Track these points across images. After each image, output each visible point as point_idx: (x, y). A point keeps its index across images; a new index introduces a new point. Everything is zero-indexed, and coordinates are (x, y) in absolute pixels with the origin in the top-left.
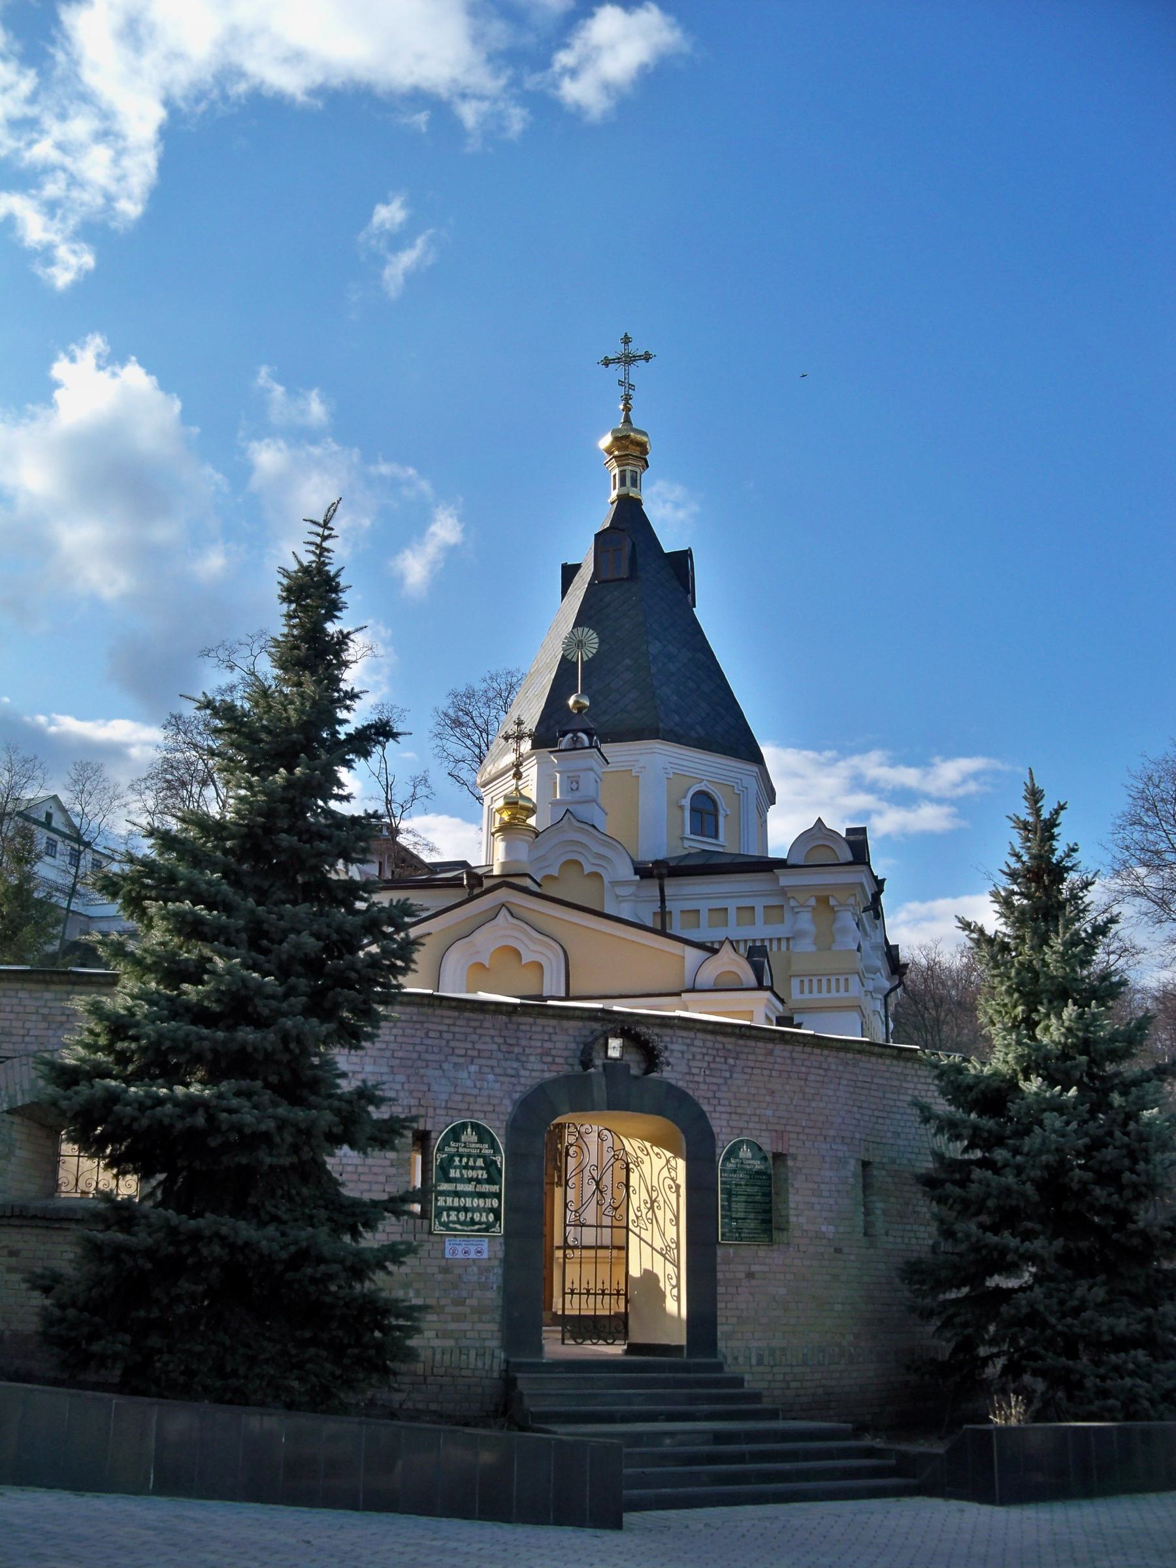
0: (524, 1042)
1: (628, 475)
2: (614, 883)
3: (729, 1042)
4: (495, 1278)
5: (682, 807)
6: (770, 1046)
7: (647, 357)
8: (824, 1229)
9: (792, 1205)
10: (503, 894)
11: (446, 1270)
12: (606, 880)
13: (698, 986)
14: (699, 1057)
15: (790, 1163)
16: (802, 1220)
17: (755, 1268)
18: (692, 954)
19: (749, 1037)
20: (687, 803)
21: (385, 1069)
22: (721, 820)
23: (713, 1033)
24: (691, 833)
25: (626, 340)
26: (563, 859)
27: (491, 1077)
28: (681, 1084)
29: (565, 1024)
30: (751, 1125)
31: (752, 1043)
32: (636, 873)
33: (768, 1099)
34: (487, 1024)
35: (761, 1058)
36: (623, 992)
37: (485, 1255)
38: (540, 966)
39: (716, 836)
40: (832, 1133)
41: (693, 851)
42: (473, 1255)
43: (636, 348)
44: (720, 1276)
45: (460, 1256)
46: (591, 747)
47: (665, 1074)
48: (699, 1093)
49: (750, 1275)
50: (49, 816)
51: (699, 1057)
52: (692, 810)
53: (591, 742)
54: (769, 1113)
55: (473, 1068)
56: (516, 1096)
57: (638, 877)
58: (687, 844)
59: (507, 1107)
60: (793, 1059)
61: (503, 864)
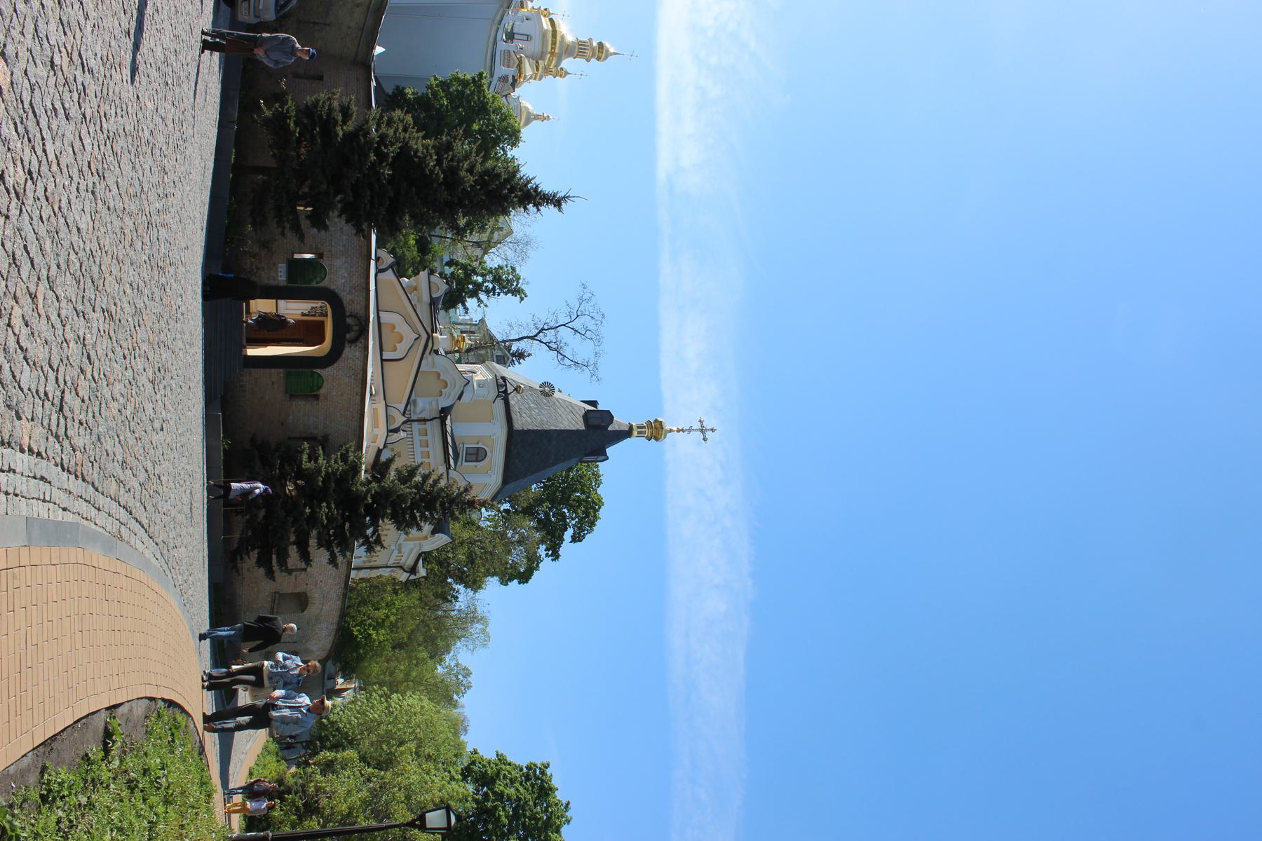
0: (356, 293)
1: (644, 430)
2: (437, 400)
3: (360, 376)
4: (272, 283)
5: (478, 443)
6: (359, 394)
7: (705, 439)
8: (291, 417)
9: (300, 403)
10: (424, 336)
11: (274, 264)
12: (439, 398)
13: (388, 408)
14: (354, 363)
15: (315, 402)
16: (294, 407)
17: (276, 386)
18: (402, 407)
19: (362, 384)
20: (480, 445)
21: (344, 243)
22: (474, 463)
23: (363, 369)
24: (467, 448)
25: (713, 430)
26: (447, 380)
27: (343, 281)
28: (343, 355)
29: (364, 309)
30: (329, 385)
31: (360, 386)
32: (442, 408)
33: (340, 393)
34: (362, 280)
35: (355, 390)
36: (385, 382)
37: (280, 279)
38: (396, 350)
39: (466, 461)
40: (327, 423)
41: (458, 449)
42: (279, 274)
43: (708, 434)
44: (273, 370)
45: (279, 269)
46: (499, 392)
47: (347, 349)
48: (340, 363)
49: (273, 383)
50: (501, 229)
51: (354, 363)
52: (478, 449)
53: (501, 392)
54: (334, 393)
55: (346, 275)
56: (337, 291)
57: (440, 409)
58: (461, 446)
59: (333, 287)
60: (355, 404)
61: (438, 338)
